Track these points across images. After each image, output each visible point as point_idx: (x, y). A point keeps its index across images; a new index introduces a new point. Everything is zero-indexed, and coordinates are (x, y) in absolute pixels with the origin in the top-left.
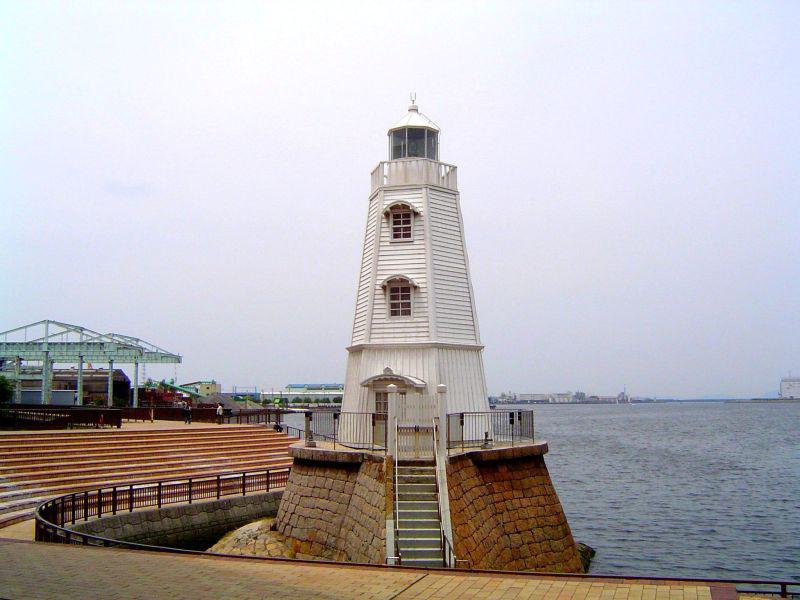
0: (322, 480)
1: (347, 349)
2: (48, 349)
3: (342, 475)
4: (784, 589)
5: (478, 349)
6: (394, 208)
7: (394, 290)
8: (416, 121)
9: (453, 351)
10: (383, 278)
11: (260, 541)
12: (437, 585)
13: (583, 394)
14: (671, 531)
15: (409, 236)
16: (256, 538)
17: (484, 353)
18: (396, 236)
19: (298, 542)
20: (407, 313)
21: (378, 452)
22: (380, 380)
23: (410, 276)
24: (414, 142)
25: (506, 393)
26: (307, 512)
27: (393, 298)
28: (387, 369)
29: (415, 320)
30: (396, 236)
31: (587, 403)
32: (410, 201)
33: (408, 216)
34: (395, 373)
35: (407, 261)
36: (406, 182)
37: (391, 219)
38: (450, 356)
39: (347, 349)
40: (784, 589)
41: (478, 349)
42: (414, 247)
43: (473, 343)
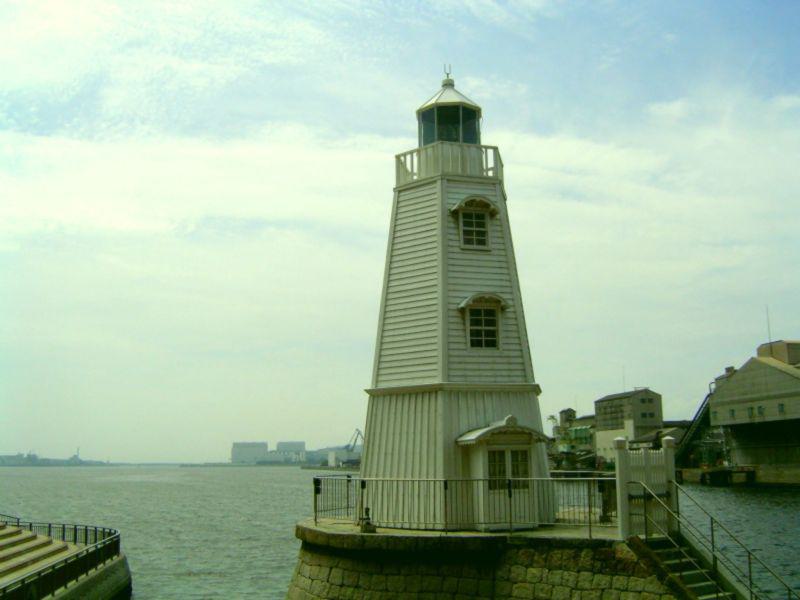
1: (367, 391)
6: (470, 203)
8: (449, 98)
20: (492, 344)
33: (481, 217)
37: (461, 220)
39: (367, 391)
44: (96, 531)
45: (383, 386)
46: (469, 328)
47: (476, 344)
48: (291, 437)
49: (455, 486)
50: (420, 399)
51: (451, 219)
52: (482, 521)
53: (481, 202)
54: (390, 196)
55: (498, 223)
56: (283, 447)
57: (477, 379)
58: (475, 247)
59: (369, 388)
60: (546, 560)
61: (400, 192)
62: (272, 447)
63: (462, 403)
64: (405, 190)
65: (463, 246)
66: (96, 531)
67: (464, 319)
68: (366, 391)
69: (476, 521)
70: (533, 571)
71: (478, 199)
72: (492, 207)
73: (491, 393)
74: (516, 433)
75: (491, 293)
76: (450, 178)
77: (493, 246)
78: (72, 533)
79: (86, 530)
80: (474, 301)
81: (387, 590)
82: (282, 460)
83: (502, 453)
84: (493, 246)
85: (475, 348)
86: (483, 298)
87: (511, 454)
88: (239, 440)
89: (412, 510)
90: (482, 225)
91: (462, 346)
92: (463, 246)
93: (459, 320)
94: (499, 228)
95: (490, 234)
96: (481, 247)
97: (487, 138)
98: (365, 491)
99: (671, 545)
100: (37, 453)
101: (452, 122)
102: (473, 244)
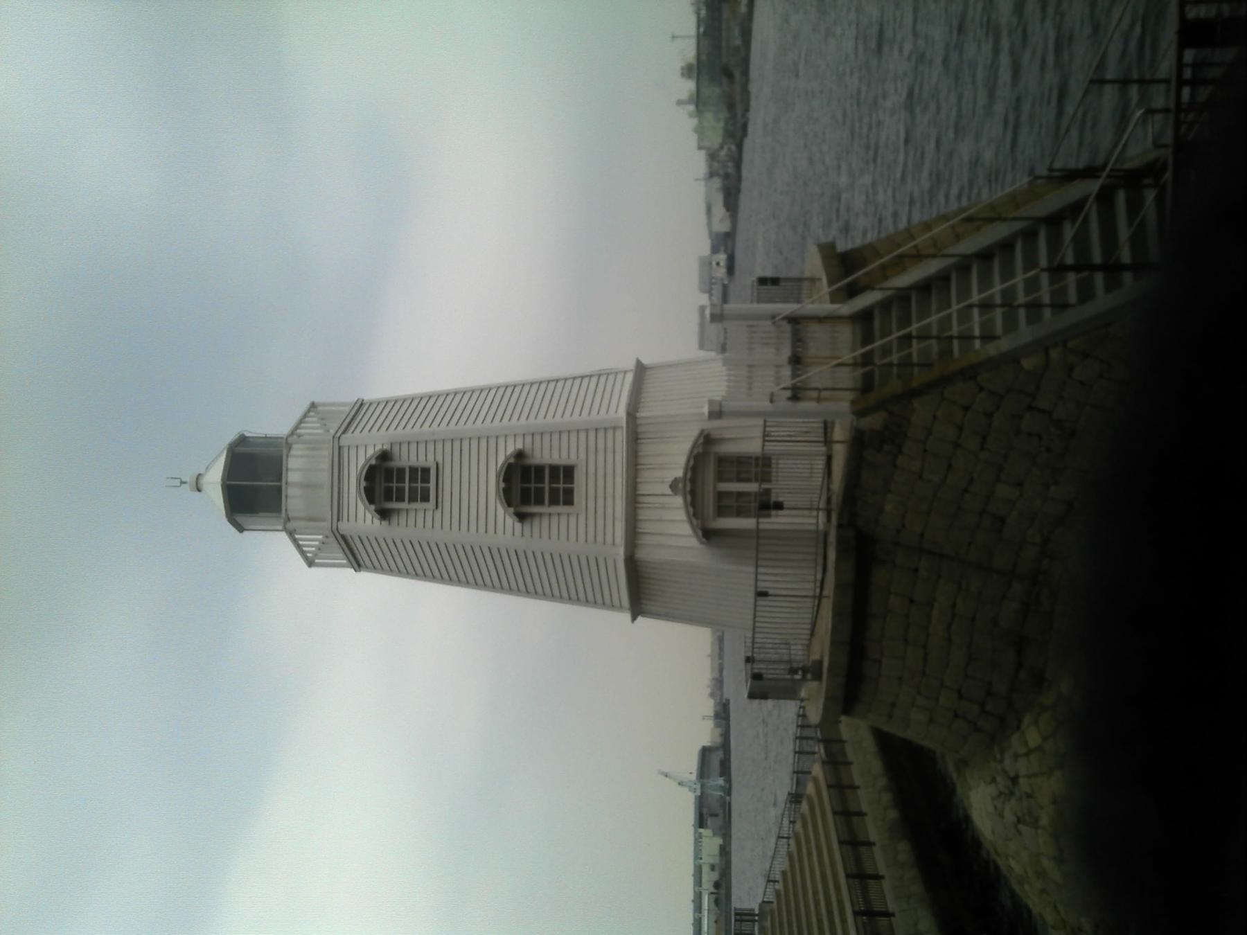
1: (634, 619)
2: (698, 13)
4: (1187, 83)
7: (525, 500)
8: (215, 476)
9: (640, 512)
11: (1022, 767)
12: (1150, 130)
13: (705, 752)
15: (426, 471)
16: (1014, 780)
17: (646, 361)
18: (425, 499)
20: (569, 501)
22: (693, 504)
23: (501, 460)
24: (253, 485)
25: (708, 691)
28: (674, 486)
30: (425, 499)
31: (726, 736)
32: (362, 461)
33: (389, 472)
34: (679, 473)
35: (474, 488)
36: (323, 520)
37: (394, 505)
39: (634, 619)
40: (1187, 83)
41: (641, 370)
42: (448, 460)
43: (630, 377)
44: (801, 738)
46: (544, 509)
47: (569, 501)
48: (690, 275)
49: (759, 547)
51: (394, 519)
52: (814, 521)
53: (366, 479)
56: (707, 285)
57: (618, 457)
58: (432, 485)
61: (359, 565)
62: (704, 299)
64: (356, 559)
65: (431, 504)
66: (801, 738)
67: (532, 515)
69: (813, 528)
71: (363, 484)
72: (373, 462)
73: (636, 477)
74: (693, 481)
75: (498, 476)
76: (335, 517)
77: (431, 457)
78: (804, 742)
80: (509, 505)
81: (900, 678)
82: (719, 841)
83: (720, 495)
84: (431, 457)
85: (576, 500)
86: (504, 490)
87: (725, 485)
88: (697, 346)
90: (401, 471)
91: (573, 519)
93: (536, 521)
94: (404, 447)
95: (413, 462)
98: (771, 592)
102: (428, 489)
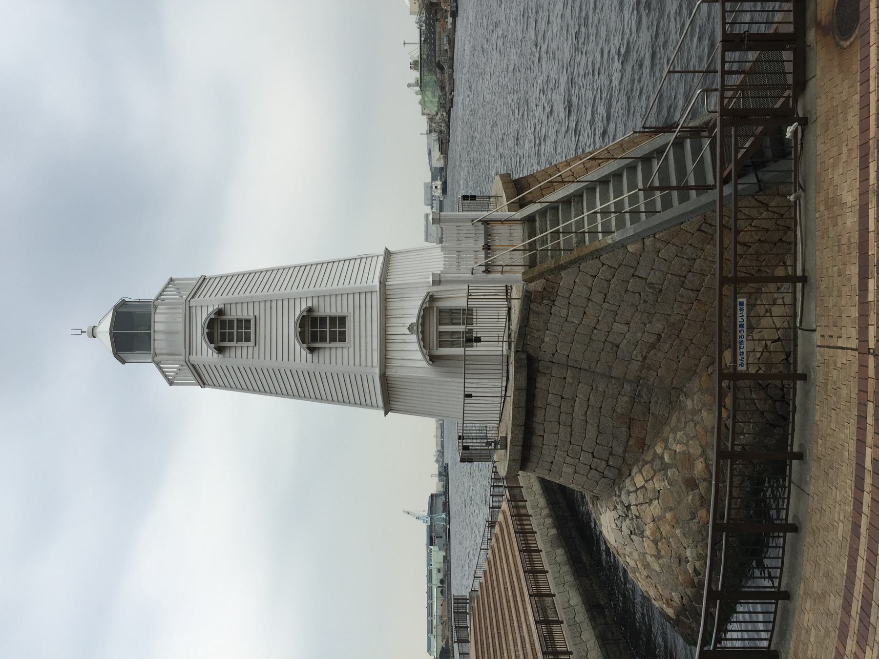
0: (550, 411)
1: (386, 414)
3: (542, 382)
5: (388, 254)
6: (211, 338)
7: (314, 339)
8: (105, 327)
10: (300, 350)
11: (632, 499)
14: (573, 114)
15: (248, 321)
16: (628, 507)
18: (248, 339)
19: (631, 442)
20: (342, 320)
21: (513, 335)
23: (298, 313)
25: (435, 458)
26: (592, 431)
27: (323, 340)
28: (410, 328)
29: (351, 310)
32: (205, 316)
33: (223, 322)
38: (391, 287)
39: (386, 414)
41: (388, 254)
43: (381, 259)
45: (381, 403)
48: (420, 195)
50: (392, 312)
51: (227, 354)
54: (207, 390)
55: (228, 307)
58: (252, 331)
59: (382, 412)
60: (538, 330)
63: (392, 312)
65: (252, 343)
68: (386, 249)
69: (501, 353)
70: (547, 339)
72: (213, 316)
74: (423, 325)
79: (494, 479)
84: (251, 313)
89: (492, 406)
92: (252, 343)
93: (321, 352)
94: (233, 306)
96: (252, 323)
97: (149, 294)
98: (474, 394)
99: (535, 255)
100: (436, 472)
101: (131, 333)
